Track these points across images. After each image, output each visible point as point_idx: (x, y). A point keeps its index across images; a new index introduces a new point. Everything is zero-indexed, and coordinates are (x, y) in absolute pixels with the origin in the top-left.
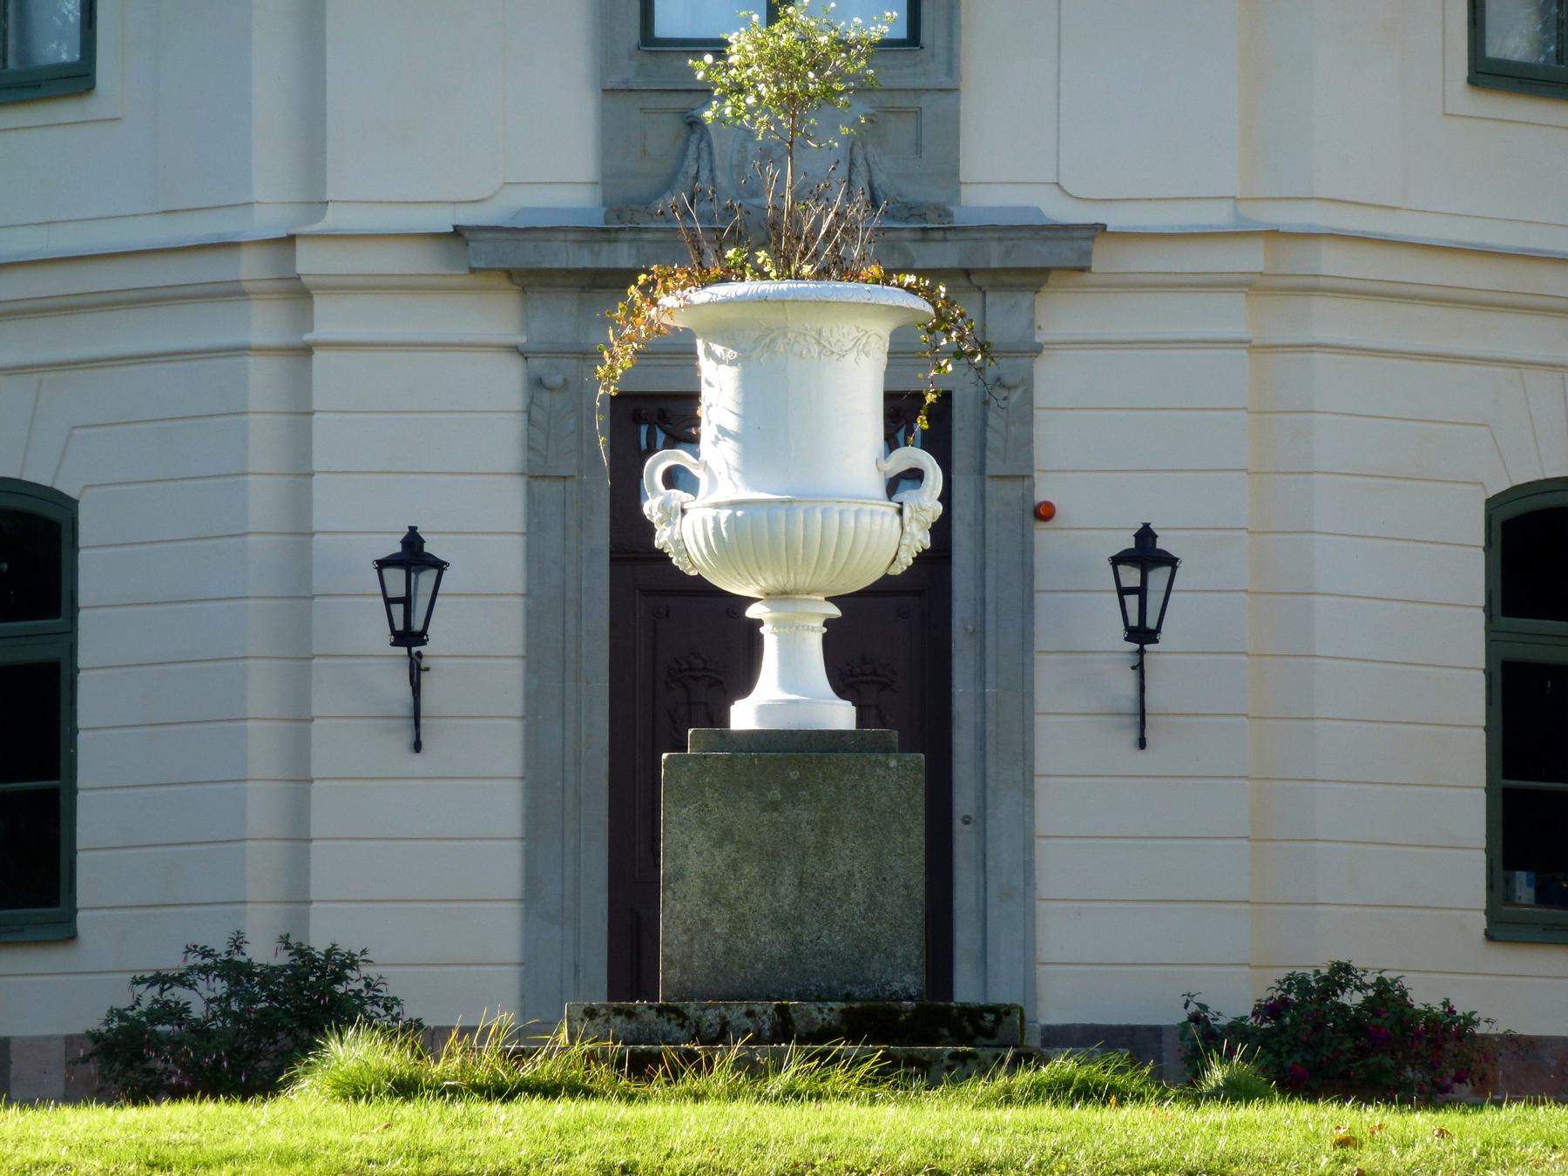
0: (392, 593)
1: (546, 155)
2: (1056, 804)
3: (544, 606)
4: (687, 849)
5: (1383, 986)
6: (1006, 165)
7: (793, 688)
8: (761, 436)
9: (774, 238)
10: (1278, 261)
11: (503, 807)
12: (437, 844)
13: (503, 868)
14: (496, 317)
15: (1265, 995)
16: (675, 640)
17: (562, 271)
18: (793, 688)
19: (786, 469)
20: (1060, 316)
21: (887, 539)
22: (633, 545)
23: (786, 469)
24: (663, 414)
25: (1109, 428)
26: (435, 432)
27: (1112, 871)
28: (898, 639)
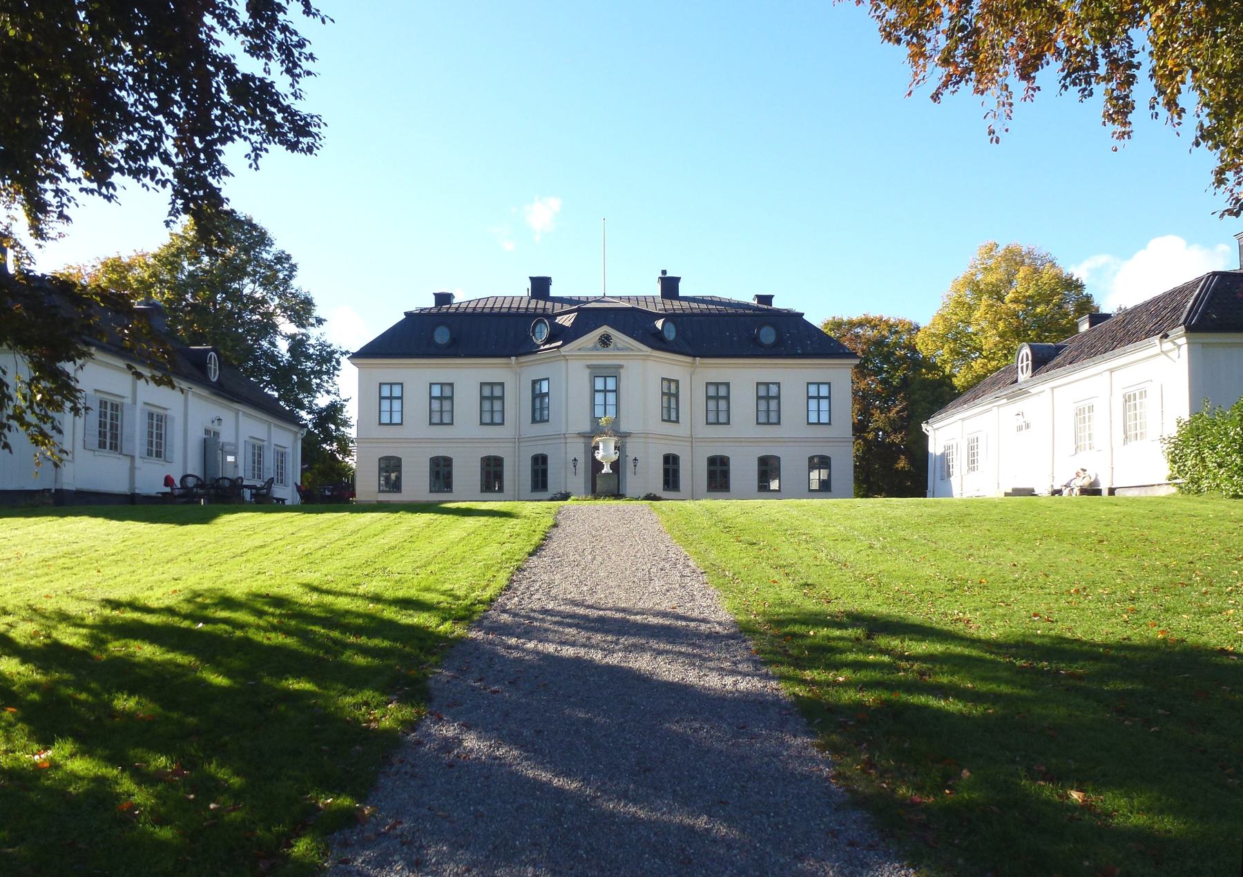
0: (383, 395)
1: (586, 427)
2: (628, 480)
3: (586, 463)
4: (599, 482)
5: (531, 349)
6: (624, 427)
7: (606, 469)
8: (604, 450)
9: (606, 434)
10: (646, 435)
11: (582, 480)
12: (578, 481)
13: (582, 485)
14: (582, 440)
15: (290, 589)
16: (597, 466)
17: (588, 436)
18: (606, 469)
19: (606, 452)
20: (628, 440)
21: (615, 458)
22: (594, 458)
23: (606, 452)
24: (597, 448)
25: (632, 449)
26: (577, 450)
27: (631, 483)
28: (615, 466)
